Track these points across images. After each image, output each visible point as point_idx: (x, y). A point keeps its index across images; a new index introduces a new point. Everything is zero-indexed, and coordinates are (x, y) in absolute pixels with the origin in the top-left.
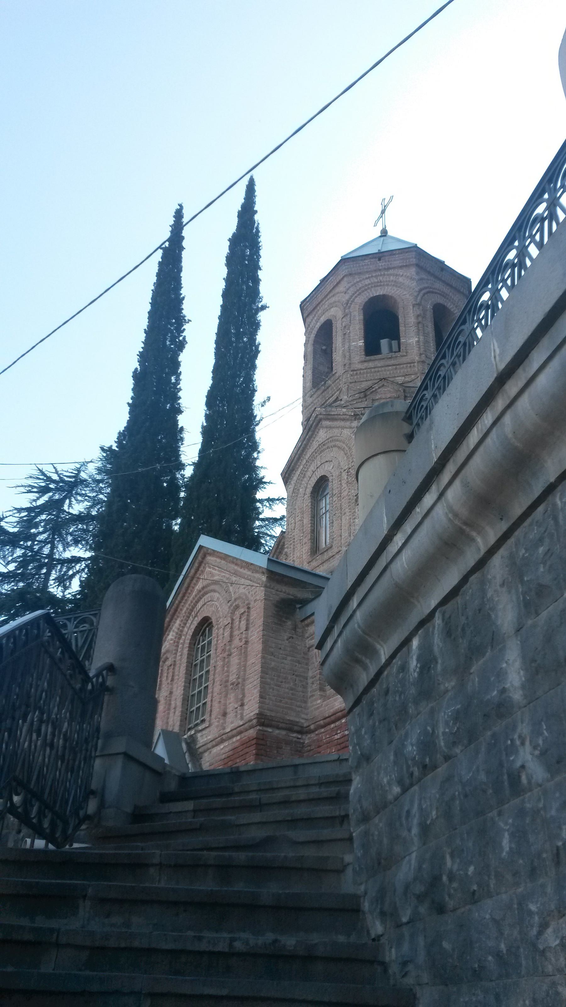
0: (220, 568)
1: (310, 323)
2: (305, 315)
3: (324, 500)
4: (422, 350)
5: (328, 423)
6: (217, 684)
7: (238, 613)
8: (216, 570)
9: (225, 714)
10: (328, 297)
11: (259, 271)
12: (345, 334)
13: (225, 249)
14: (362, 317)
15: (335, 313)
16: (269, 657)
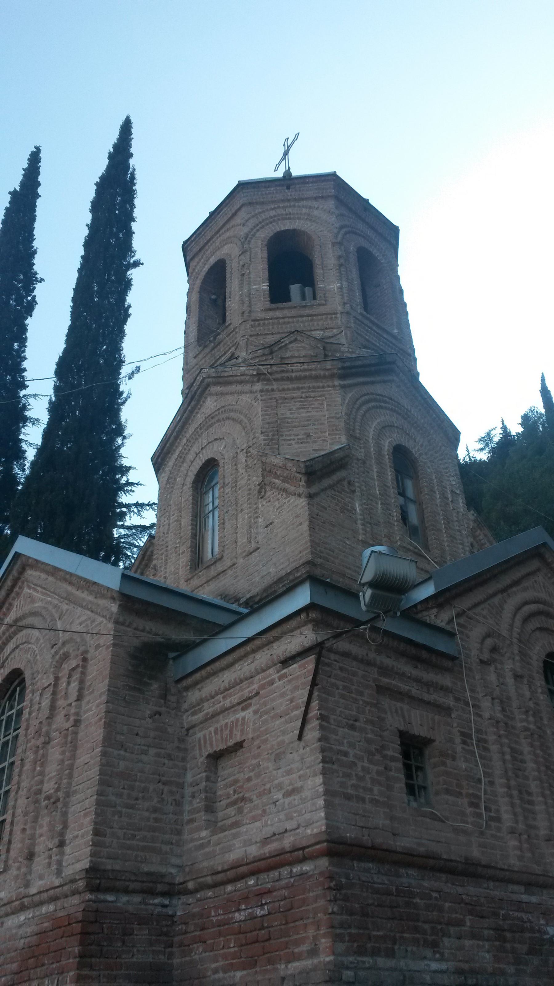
0: (44, 588)
1: (196, 266)
2: (189, 258)
3: (211, 493)
4: (346, 299)
5: (218, 389)
6: (23, 792)
7: (67, 667)
8: (38, 592)
9: (30, 856)
10: (221, 233)
11: (132, 223)
12: (243, 275)
13: (91, 193)
14: (265, 255)
15: (229, 251)
16: (116, 752)
